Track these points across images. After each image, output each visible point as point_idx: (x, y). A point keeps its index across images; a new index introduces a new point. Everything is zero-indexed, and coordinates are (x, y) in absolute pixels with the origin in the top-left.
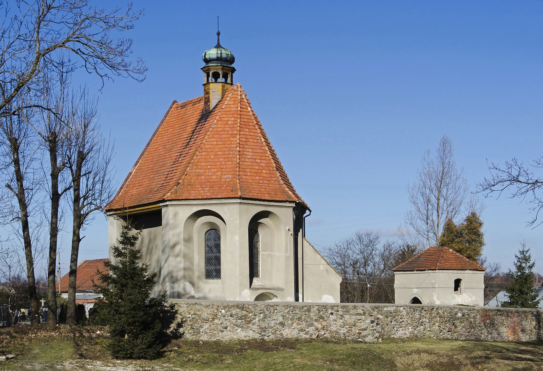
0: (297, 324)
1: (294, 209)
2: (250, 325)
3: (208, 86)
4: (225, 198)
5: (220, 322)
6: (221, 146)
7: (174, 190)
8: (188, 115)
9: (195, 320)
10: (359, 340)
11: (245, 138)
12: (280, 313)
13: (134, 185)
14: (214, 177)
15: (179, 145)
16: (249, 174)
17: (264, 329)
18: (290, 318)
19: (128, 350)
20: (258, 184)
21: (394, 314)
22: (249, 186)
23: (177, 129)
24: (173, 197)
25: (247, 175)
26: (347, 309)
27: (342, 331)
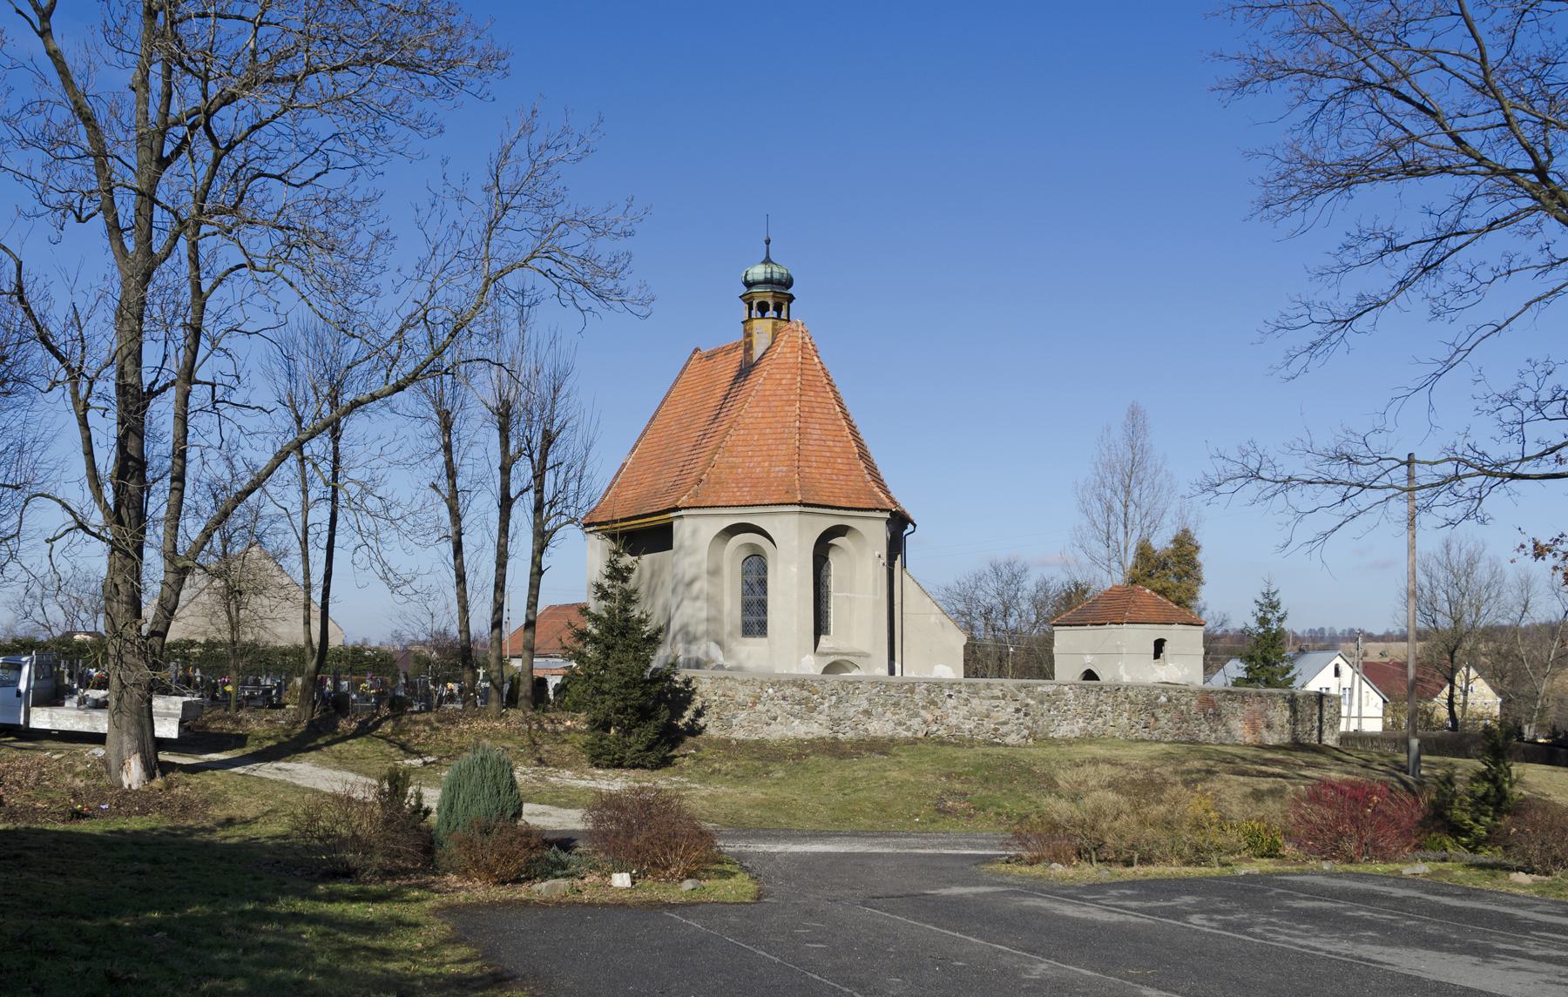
1: (888, 522)
2: (815, 714)
5: (766, 708)
6: (769, 420)
9: (724, 705)
14: (758, 470)
19: (615, 753)
24: (692, 502)
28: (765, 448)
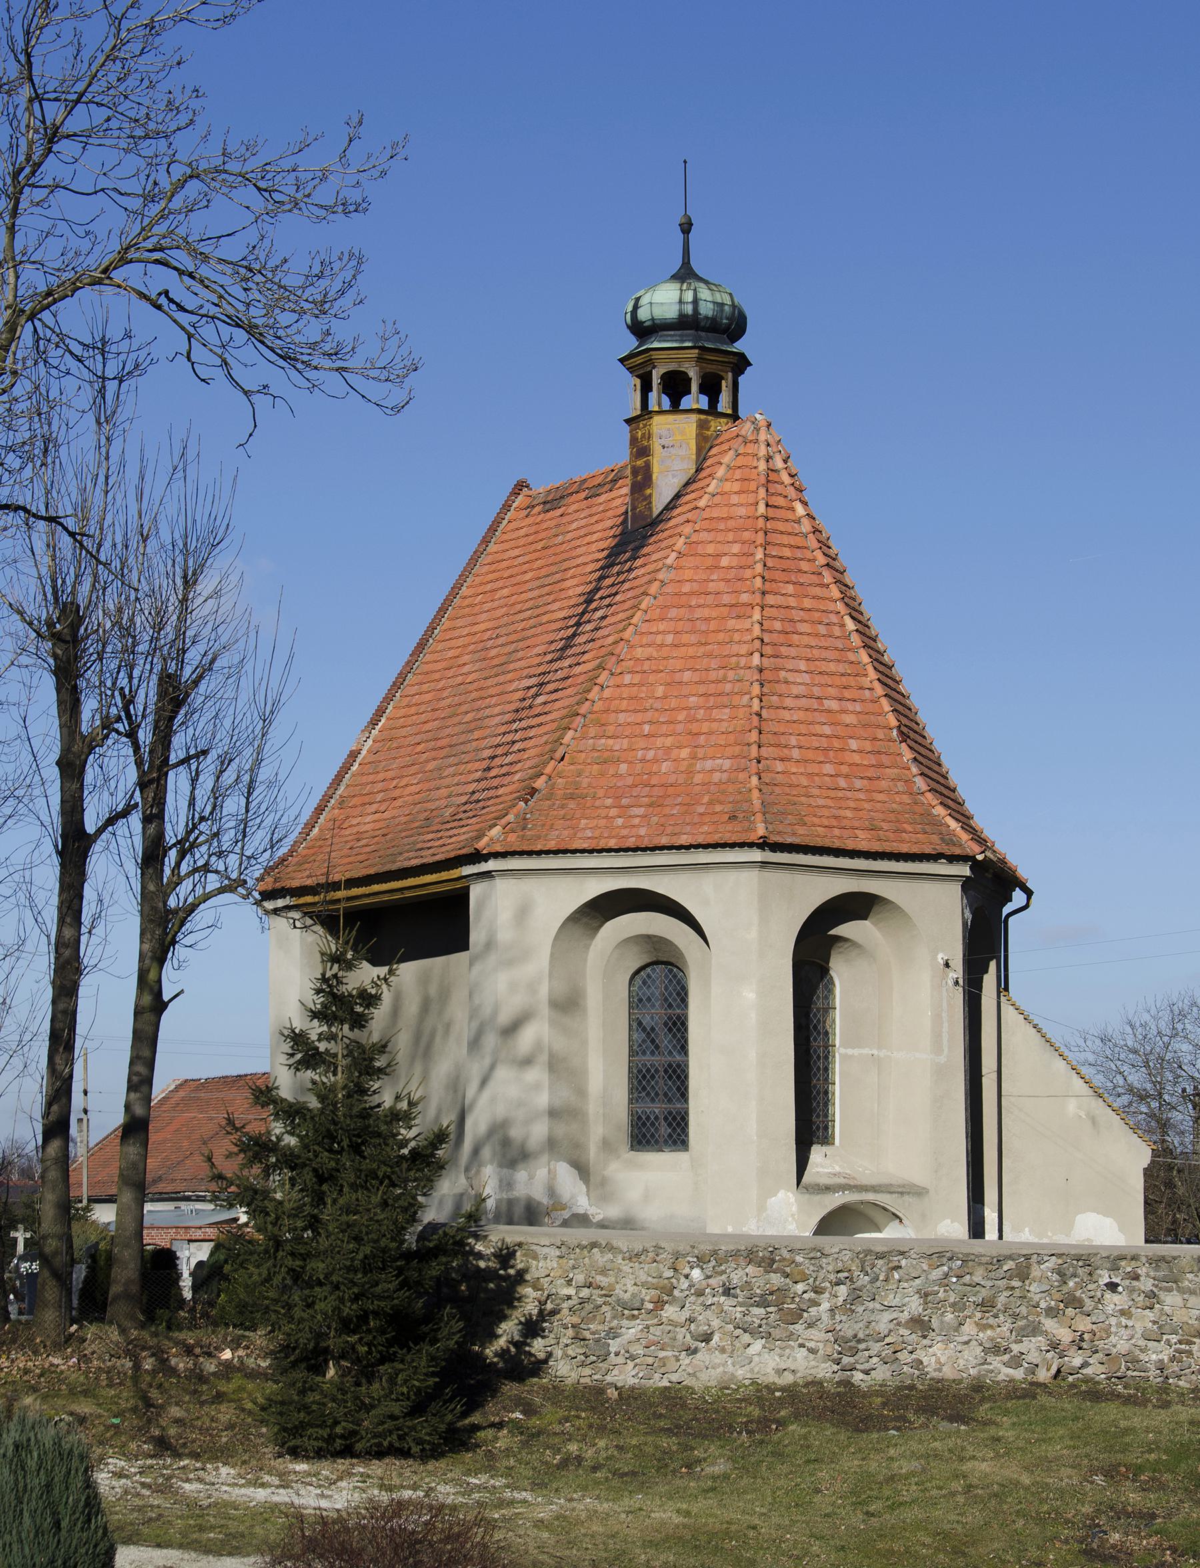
0: (977, 1324)
2: (799, 1328)
3: (645, 426)
4: (706, 846)
5: (686, 1314)
6: (691, 651)
7: (516, 816)
8: (569, 536)
9: (589, 1307)
11: (782, 620)
12: (911, 1283)
14: (665, 767)
15: (535, 646)
16: (796, 753)
18: (952, 1300)
19: (336, 1423)
20: (832, 794)
24: (514, 842)
25: (789, 760)
26: (1171, 1271)
27: (1154, 1357)
28: (681, 716)
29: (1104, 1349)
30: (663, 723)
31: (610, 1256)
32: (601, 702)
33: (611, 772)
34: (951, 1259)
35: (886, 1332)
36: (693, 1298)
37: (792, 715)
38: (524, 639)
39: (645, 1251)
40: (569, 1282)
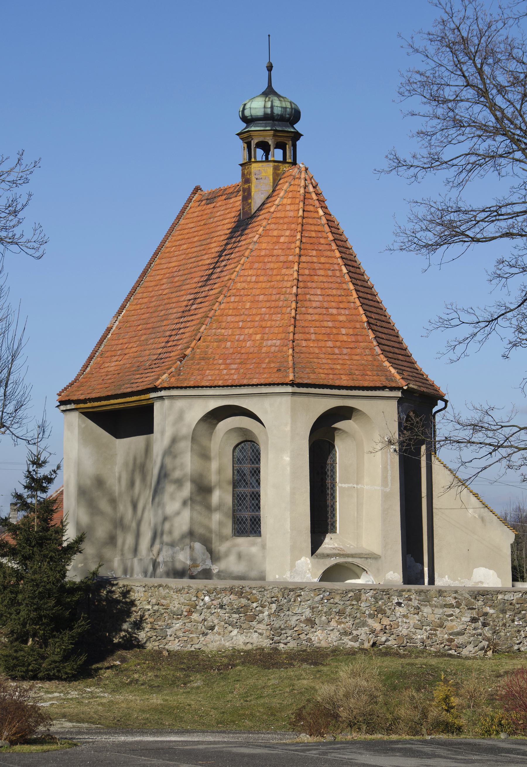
0: (337, 622)
1: (400, 401)
2: (254, 623)
3: (248, 168)
4: (265, 385)
5: (202, 617)
6: (264, 285)
7: (176, 368)
8: (216, 219)
9: (158, 614)
10: (450, 652)
11: (309, 269)
12: (306, 603)
13: (113, 353)
14: (249, 344)
15: (195, 278)
16: (313, 337)
17: (278, 631)
18: (325, 610)
19: (29, 664)
20: (331, 357)
21: (518, 606)
22: (311, 360)
23: (196, 244)
24: (173, 382)
25: (309, 340)
26: (426, 596)
27: (419, 637)
28: (257, 318)
29: (396, 633)
30: (249, 321)
31: (168, 591)
32: (219, 311)
33: (223, 346)
34: (324, 591)
35: (294, 625)
36: (205, 610)
37: (312, 317)
38: (191, 273)
39: (183, 588)
40: (149, 603)
